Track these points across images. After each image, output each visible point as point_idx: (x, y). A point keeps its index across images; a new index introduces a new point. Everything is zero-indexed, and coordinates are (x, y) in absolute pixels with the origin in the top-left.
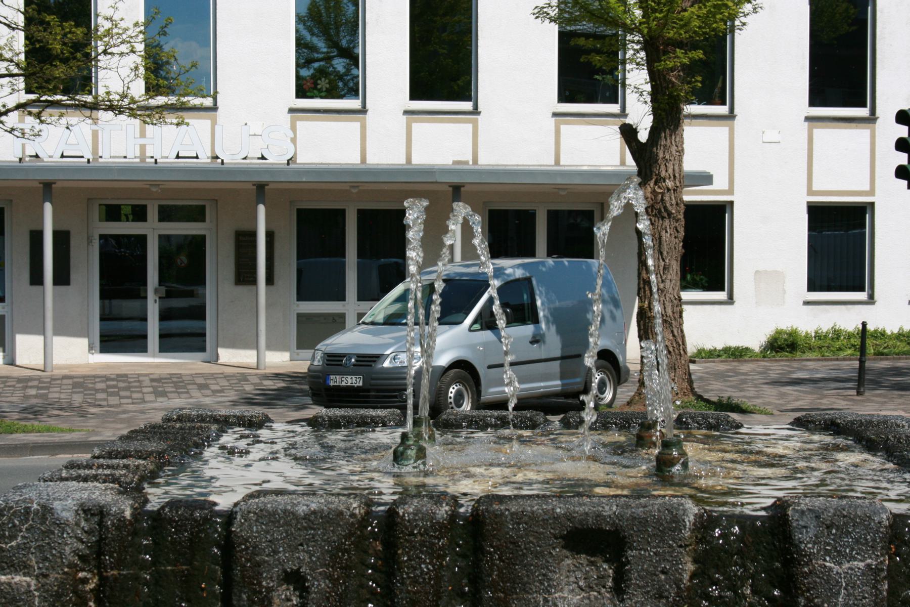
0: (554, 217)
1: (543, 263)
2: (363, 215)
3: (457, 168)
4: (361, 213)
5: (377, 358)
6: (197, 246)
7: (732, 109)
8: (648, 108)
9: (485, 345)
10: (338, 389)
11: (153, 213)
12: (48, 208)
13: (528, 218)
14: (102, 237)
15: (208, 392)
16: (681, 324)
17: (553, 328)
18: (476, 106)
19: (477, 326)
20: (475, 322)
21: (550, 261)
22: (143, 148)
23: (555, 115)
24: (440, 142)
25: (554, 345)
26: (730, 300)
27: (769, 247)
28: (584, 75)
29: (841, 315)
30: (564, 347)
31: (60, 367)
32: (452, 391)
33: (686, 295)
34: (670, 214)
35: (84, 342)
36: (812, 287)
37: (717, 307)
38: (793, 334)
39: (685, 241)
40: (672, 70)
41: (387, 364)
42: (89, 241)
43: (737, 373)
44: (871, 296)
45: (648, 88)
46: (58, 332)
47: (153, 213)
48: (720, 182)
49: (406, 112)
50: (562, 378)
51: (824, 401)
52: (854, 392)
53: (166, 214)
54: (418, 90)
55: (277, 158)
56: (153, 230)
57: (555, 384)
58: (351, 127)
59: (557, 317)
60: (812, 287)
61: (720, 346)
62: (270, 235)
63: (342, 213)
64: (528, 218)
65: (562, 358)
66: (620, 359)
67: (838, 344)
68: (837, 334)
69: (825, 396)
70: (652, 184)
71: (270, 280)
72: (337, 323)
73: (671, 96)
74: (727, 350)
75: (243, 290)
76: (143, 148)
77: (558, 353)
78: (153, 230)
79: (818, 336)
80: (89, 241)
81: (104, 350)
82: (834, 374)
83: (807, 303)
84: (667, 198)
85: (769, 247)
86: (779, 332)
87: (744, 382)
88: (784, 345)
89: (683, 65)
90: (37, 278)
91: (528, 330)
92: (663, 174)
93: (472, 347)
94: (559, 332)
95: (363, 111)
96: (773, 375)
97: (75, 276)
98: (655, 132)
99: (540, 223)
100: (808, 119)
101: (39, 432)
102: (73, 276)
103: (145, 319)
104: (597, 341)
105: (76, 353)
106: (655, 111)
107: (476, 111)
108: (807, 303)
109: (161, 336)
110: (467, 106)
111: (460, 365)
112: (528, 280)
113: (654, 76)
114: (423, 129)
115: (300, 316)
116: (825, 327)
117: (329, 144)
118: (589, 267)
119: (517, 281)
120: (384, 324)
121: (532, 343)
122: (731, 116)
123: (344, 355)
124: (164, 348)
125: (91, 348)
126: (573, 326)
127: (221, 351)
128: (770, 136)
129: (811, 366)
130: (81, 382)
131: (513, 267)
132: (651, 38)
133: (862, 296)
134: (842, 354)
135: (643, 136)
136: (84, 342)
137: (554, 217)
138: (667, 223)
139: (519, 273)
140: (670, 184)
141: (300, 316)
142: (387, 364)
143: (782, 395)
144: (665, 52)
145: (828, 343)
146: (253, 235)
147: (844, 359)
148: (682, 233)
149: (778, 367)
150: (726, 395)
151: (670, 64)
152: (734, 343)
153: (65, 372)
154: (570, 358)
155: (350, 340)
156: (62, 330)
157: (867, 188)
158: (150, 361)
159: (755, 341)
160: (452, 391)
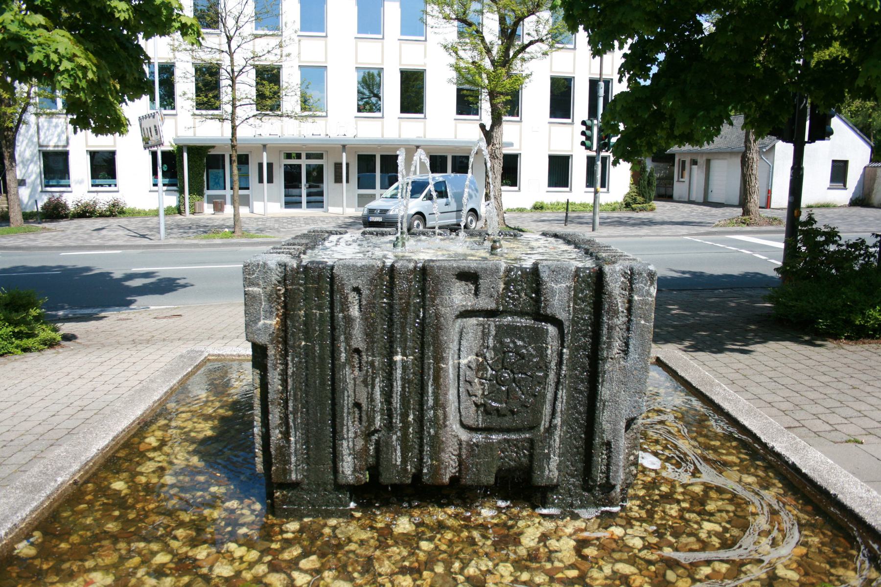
0: (454, 158)
2: (382, 156)
6: (320, 168)
11: (304, 156)
13: (444, 158)
21: (453, 175)
25: (453, 206)
28: (466, 104)
29: (559, 196)
35: (279, 204)
53: (309, 156)
54: (404, 109)
64: (444, 158)
71: (347, 181)
75: (338, 185)
78: (304, 162)
96: (535, 218)
99: (449, 162)
116: (554, 201)
131: (439, 177)
136: (279, 204)
137: (454, 158)
139: (441, 179)
149: (537, 215)
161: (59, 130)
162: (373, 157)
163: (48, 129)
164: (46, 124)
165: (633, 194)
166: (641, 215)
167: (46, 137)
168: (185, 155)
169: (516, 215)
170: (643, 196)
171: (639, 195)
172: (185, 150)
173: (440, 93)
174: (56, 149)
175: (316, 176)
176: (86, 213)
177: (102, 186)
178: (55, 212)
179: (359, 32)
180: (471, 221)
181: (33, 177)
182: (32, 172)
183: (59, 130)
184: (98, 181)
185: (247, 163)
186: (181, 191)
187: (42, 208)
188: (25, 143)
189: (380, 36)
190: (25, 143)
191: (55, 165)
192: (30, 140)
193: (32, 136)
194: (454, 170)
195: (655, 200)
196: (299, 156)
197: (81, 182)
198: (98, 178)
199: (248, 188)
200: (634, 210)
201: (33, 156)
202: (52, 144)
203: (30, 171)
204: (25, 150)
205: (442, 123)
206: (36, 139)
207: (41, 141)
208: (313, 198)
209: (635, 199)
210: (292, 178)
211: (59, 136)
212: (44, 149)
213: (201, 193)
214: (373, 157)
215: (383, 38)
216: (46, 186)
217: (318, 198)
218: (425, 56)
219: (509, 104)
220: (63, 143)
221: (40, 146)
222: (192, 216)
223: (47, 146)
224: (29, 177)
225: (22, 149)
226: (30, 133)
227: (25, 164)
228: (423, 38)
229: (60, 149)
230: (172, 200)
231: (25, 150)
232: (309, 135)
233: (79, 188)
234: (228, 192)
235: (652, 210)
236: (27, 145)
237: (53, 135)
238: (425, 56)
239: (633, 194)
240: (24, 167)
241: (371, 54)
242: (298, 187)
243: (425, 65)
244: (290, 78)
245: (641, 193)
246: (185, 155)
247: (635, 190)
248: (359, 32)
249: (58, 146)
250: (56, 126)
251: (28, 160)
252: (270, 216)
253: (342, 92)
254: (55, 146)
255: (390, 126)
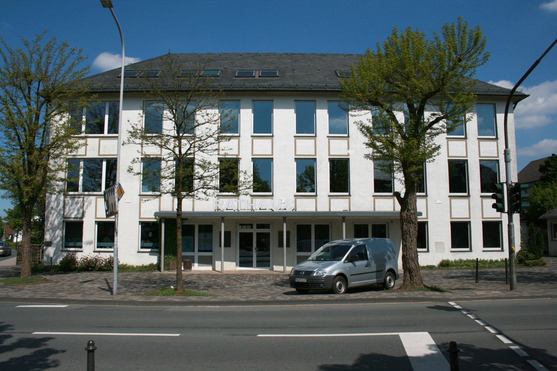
0: (374, 227)
1: (370, 240)
2: (316, 226)
3: (345, 212)
4: (316, 226)
5: (312, 272)
6: (267, 235)
7: (426, 194)
8: (403, 186)
9: (349, 267)
10: (298, 283)
11: (255, 226)
12: (223, 224)
13: (366, 227)
14: (240, 233)
15: (265, 280)
16: (418, 260)
17: (374, 261)
18: (350, 194)
19: (346, 261)
20: (346, 259)
21: (372, 239)
22: (252, 206)
23: (373, 196)
24: (339, 205)
25: (374, 267)
26: (428, 251)
27: (439, 234)
28: (382, 185)
29: (463, 255)
30: (377, 267)
31: (226, 271)
32: (338, 284)
33: (419, 250)
34: (413, 222)
35: (235, 263)
36: (453, 247)
37: (424, 253)
38: (448, 261)
39: (418, 231)
40: (412, 172)
41: (315, 275)
42: (236, 234)
43: (432, 274)
44: (471, 249)
45: (403, 179)
46: (225, 260)
47: (255, 226)
48: (424, 216)
49: (329, 196)
50: (376, 278)
51: (465, 285)
52: (474, 281)
53: (259, 226)
54: (333, 189)
55: (289, 209)
56: (255, 231)
57: (374, 281)
58: (313, 201)
59: (375, 257)
60: (453, 247)
61: (425, 265)
62: (288, 233)
63: (310, 226)
64: (366, 227)
65: (377, 272)
66: (396, 271)
67: (461, 264)
68: (461, 261)
69: (465, 283)
70: (406, 212)
71: (288, 245)
72: (305, 258)
73: (412, 181)
74: (428, 266)
75: (280, 248)
76: (252, 206)
77: (375, 270)
78: (255, 231)
79: (455, 262)
80: (236, 234)
81: (240, 266)
82: (463, 274)
83: (451, 252)
84: (411, 216)
85: (439, 234)
86: (443, 261)
87: (435, 277)
88: (445, 264)
89: (415, 171)
90: (281, 245)
91: (365, 262)
92: (410, 208)
93: (345, 268)
94: (375, 262)
95: (316, 196)
96: (444, 275)
97: (232, 245)
98: (406, 194)
99: (369, 227)
100: (449, 196)
101: (198, 295)
102: (232, 245)
103: (252, 257)
104: (388, 267)
105: (231, 267)
106: (406, 187)
107: (350, 195)
108: (451, 252)
109: (257, 262)
110: (347, 194)
111: (340, 274)
112: (364, 245)
113: (406, 175)
114: (334, 201)
115: (298, 256)
116: (457, 259)
117: (306, 205)
118: (385, 240)
119: (361, 245)
120: (316, 260)
121: (366, 267)
122: (426, 196)
123: (300, 271)
124: (258, 266)
125: (236, 265)
126: (380, 261)
127: (274, 266)
128: (438, 201)
129: (455, 272)
130: (230, 277)
131: (359, 241)
132: (404, 161)
133: (468, 249)
134: (463, 267)
135: (402, 196)
136: (235, 263)
137: (374, 227)
138: (412, 225)
139: (361, 243)
140: (412, 212)
141: (298, 256)
142: (315, 275)
143: (449, 283)
144: (409, 166)
145: (460, 264)
146: (282, 232)
147: (464, 269)
148: (417, 229)
149: (444, 272)
150: (434, 285)
151: (411, 170)
152: (430, 264)
153: (227, 273)
154: (379, 271)
155: (306, 265)
156: (227, 260)
157: (468, 217)
158: (254, 269)
159: (436, 263)
160: (338, 284)
161: (79, 205)
162: (309, 227)
163: (72, 205)
164: (70, 201)
165: (525, 252)
166: (536, 269)
167: (69, 210)
168: (163, 225)
169: (427, 272)
170: (534, 254)
171: (530, 252)
172: (163, 220)
173: (362, 174)
174: (75, 220)
175: (264, 245)
176: (90, 266)
177: (105, 247)
178: (69, 266)
179: (297, 133)
180: (390, 280)
181: (58, 239)
182: (58, 236)
183: (79, 205)
184: (102, 244)
185: (211, 231)
186: (160, 253)
187: (60, 263)
188: (55, 215)
189: (314, 135)
190: (55, 215)
191: (73, 231)
192: (59, 213)
193: (60, 210)
194: (374, 235)
195: (544, 256)
196: (252, 226)
197: (90, 243)
198: (102, 242)
199: (211, 251)
200: (527, 265)
201: (59, 224)
202: (73, 216)
203: (56, 235)
204: (55, 219)
205: (363, 197)
206: (62, 213)
207: (65, 213)
208: (261, 258)
209: (527, 256)
210: (245, 241)
211: (78, 210)
212: (67, 220)
213: (175, 253)
214: (309, 227)
215: (316, 136)
216: (66, 247)
217: (266, 258)
218: (348, 149)
219: (417, 183)
220: (80, 216)
221: (64, 217)
222: (167, 272)
223: (70, 218)
224: (55, 239)
225: (53, 219)
226: (59, 208)
227: (54, 229)
228: (346, 135)
229: (78, 220)
230: (154, 260)
231: (55, 219)
232: (257, 209)
233: (88, 249)
234: (196, 254)
235: (544, 264)
236: (56, 216)
237: (74, 209)
238: (348, 149)
239: (525, 252)
240: (52, 232)
241: (306, 147)
242: (250, 250)
243: (348, 155)
244: (246, 169)
245: (531, 250)
246: (163, 225)
247: (526, 248)
248: (297, 133)
249: (77, 218)
250: (77, 203)
251: (56, 226)
252: (225, 273)
253: (284, 178)
254: (74, 218)
255: (323, 201)
